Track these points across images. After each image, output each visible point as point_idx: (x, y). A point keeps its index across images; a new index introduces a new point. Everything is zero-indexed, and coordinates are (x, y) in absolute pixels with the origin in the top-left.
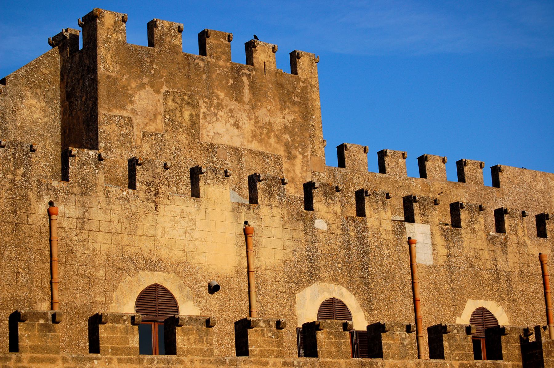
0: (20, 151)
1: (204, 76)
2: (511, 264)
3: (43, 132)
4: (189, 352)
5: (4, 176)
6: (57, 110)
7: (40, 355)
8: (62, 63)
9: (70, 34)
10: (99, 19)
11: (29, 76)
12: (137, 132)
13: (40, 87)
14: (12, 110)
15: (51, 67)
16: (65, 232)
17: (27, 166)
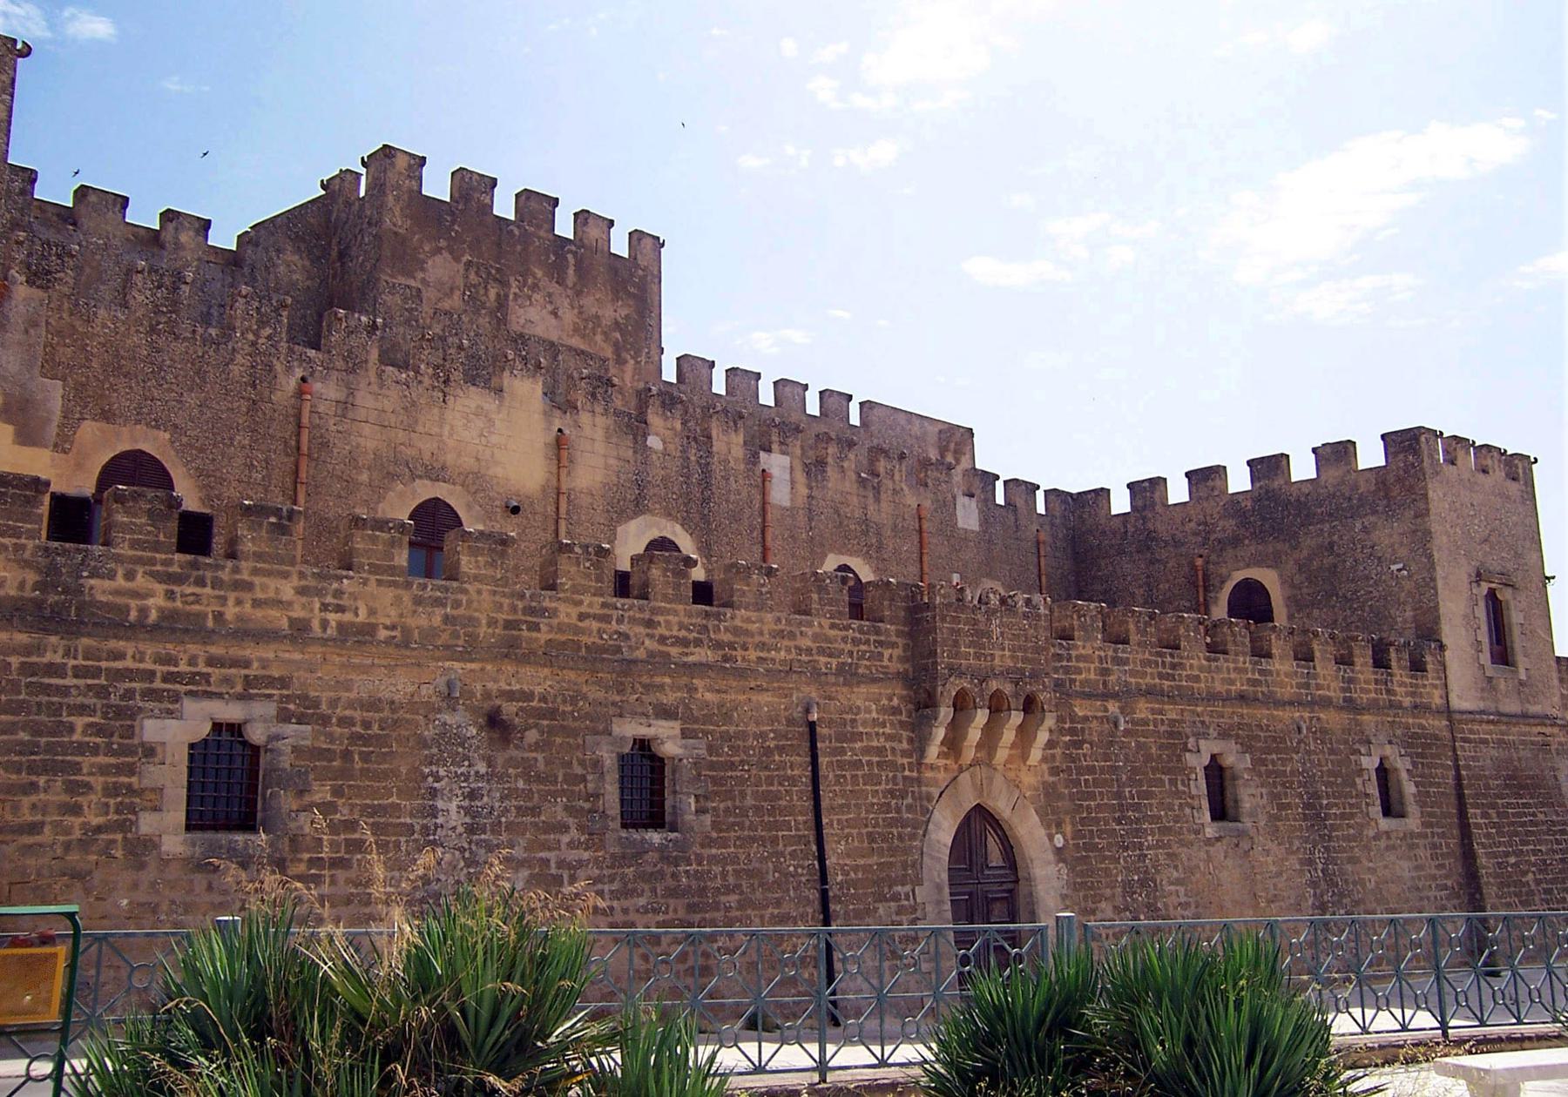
1: (519, 248)
2: (884, 515)
4: (476, 578)
7: (266, 566)
12: (427, 309)
16: (320, 418)
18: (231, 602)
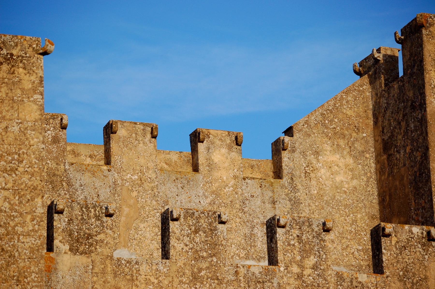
0: (308, 232)
3: (351, 202)
5: (287, 269)
6: (371, 167)
8: (374, 99)
9: (384, 56)
10: (426, 29)
11: (327, 122)
13: (343, 136)
14: (304, 172)
15: (359, 106)
17: (319, 253)
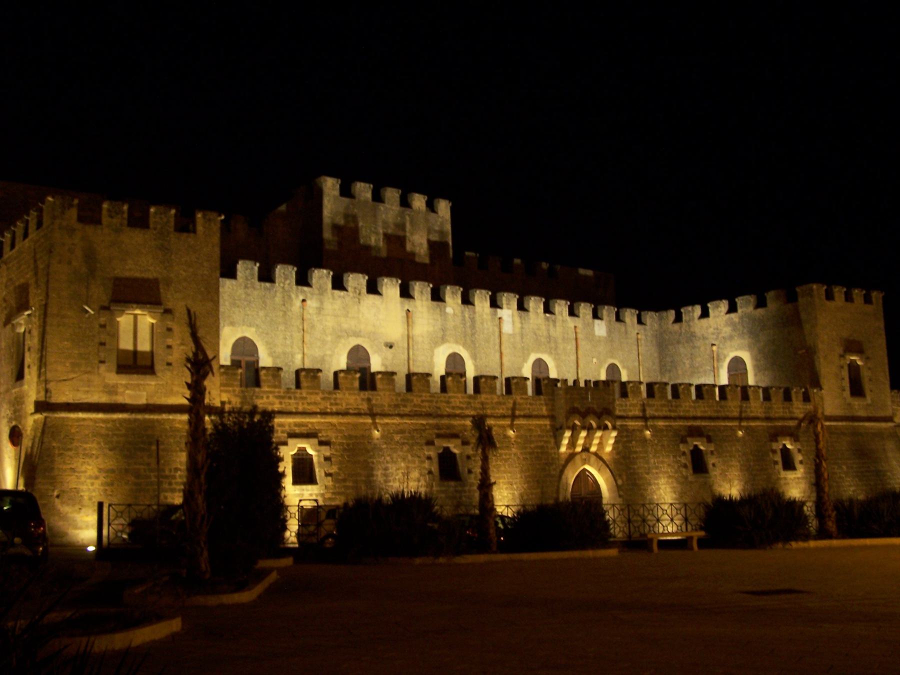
18: (300, 404)
